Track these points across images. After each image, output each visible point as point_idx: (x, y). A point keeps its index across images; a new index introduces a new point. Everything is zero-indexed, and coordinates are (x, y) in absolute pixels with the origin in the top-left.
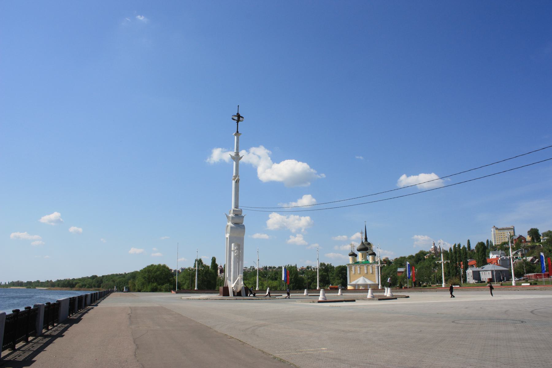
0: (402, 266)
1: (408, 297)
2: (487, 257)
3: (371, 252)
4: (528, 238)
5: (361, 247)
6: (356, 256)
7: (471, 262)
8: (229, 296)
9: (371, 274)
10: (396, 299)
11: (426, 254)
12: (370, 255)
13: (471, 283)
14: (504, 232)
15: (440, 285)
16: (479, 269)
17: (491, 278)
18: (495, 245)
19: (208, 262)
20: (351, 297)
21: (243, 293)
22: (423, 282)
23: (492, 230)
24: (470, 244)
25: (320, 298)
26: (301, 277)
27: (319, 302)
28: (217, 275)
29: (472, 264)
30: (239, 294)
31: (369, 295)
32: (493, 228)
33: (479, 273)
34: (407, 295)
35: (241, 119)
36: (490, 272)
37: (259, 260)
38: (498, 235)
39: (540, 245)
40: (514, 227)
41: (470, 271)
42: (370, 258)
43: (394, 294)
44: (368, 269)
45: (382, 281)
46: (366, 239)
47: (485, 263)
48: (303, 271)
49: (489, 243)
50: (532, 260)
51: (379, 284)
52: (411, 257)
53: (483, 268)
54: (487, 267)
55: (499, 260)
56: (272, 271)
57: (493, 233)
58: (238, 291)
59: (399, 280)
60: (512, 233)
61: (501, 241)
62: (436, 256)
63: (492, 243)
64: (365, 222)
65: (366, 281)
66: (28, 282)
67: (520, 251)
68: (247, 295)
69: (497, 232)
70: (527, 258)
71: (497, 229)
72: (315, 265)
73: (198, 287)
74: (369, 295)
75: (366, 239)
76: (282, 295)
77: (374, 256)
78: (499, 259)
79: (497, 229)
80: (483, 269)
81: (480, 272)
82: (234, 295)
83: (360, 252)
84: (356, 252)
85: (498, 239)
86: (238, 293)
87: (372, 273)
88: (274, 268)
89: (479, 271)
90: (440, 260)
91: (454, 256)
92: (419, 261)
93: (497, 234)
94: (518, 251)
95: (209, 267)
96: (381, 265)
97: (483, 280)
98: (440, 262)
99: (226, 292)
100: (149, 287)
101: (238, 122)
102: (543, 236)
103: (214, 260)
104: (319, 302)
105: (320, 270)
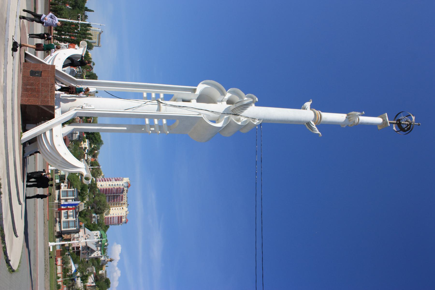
14: (97, 38)
23: (100, 30)
24: (90, 11)
32: (101, 31)
38: (95, 33)
40: (100, 47)
49: (89, 28)
55: (73, 69)
57: (97, 29)
60: (95, 45)
67: (80, 71)
69: (98, 33)
71: (100, 33)
79: (100, 33)
91: (80, 35)
93: (96, 38)
94: (80, 69)
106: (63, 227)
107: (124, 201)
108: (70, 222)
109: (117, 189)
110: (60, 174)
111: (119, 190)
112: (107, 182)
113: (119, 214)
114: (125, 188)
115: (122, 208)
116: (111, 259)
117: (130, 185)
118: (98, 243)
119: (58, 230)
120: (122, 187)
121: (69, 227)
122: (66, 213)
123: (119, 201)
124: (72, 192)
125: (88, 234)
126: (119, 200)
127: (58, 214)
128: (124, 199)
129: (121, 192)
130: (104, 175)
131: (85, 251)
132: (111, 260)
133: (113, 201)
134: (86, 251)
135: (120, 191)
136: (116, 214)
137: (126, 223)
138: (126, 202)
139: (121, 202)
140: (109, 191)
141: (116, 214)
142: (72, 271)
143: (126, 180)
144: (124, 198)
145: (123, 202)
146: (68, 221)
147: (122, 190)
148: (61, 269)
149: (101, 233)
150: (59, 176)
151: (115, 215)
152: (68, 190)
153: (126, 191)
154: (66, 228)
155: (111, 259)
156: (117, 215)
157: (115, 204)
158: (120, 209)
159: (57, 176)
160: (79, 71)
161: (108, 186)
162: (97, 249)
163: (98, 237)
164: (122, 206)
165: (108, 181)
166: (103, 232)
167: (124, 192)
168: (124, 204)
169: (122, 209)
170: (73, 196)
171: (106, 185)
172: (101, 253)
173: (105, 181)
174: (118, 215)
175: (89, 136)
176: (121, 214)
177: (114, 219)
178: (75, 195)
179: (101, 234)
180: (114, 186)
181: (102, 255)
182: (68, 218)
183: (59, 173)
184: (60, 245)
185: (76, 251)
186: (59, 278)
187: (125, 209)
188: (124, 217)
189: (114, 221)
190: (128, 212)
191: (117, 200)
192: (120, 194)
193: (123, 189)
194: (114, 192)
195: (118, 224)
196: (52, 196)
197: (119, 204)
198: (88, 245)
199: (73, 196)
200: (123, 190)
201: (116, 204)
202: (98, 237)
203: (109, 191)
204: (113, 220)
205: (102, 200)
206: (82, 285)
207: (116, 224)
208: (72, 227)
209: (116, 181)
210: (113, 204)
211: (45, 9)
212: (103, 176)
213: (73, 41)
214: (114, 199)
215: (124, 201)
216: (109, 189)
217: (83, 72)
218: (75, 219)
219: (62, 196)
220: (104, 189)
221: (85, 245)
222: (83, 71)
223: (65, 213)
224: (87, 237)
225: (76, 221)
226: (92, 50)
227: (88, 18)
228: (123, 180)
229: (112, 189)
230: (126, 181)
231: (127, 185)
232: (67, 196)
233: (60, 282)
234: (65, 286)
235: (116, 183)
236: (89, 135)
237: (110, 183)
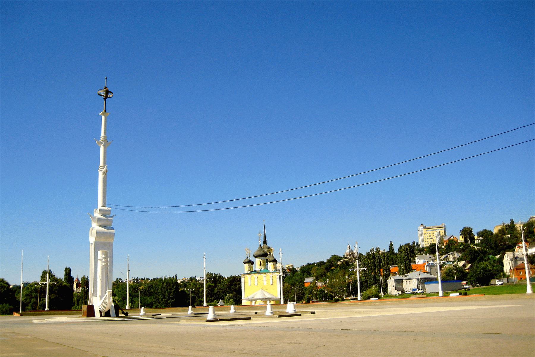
0: (309, 275)
1: (314, 313)
2: (412, 262)
3: (271, 259)
4: (461, 239)
5: (257, 253)
6: (252, 263)
7: (393, 268)
8: (95, 316)
9: (114, 229)
10: (300, 315)
11: (340, 260)
12: (270, 262)
14: (433, 231)
15: (356, 298)
16: (401, 277)
18: (422, 247)
19: (60, 275)
20: (415, 305)
21: (113, 312)
22: (336, 295)
25: (210, 316)
26: (183, 291)
27: (208, 321)
28: (73, 291)
29: (394, 271)
30: (107, 314)
31: (268, 311)
34: (313, 311)
35: (110, 95)
36: (416, 280)
37: (129, 270)
39: (474, 246)
41: (391, 281)
42: (271, 265)
43: (298, 310)
45: (284, 295)
46: (265, 242)
47: (409, 269)
48: (185, 284)
50: (464, 266)
51: (281, 298)
52: (321, 264)
54: (411, 275)
55: (426, 266)
56: (145, 283)
58: (106, 310)
59: (307, 293)
60: (443, 232)
61: (430, 243)
63: (419, 245)
65: (264, 295)
68: (117, 315)
70: (459, 263)
72: (201, 276)
73: (49, 307)
74: (268, 311)
75: (265, 242)
76: (160, 315)
77: (275, 263)
78: (427, 265)
80: (407, 278)
82: (101, 316)
84: (252, 259)
85: (427, 240)
86: (106, 313)
88: (148, 279)
90: (355, 267)
95: (61, 280)
96: (284, 275)
98: (355, 270)
99: (90, 312)
101: (105, 99)
102: (479, 236)
103: (68, 271)
104: (208, 321)
105: (207, 282)
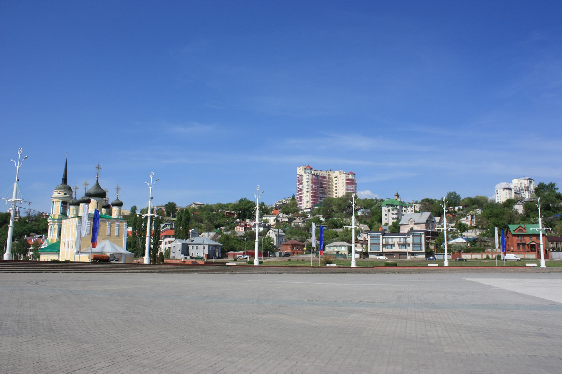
13: (178, 258)
17: (207, 254)
33: (356, 258)
44: (112, 227)
53: (192, 241)
62: (29, 220)
64: (67, 153)
65: (116, 249)
66: (70, 261)
67: (170, 224)
81: (189, 246)
83: (94, 199)
87: (118, 236)
89: (188, 244)
92: (4, 225)
97: (192, 255)
100: (251, 204)
106: (378, 250)
107: (326, 175)
108: (415, 242)
109: (313, 183)
110: (347, 253)
111: (315, 180)
112: (303, 195)
113: (343, 183)
114: (311, 173)
115: (335, 178)
116: (395, 196)
117: (308, 166)
118: (399, 209)
119: (423, 256)
120: (311, 177)
121: (421, 244)
122: (400, 246)
123: (326, 182)
124: (373, 238)
125: (409, 221)
126: (324, 181)
127: (402, 256)
128: (324, 174)
129: (316, 178)
130: (284, 199)
131: (430, 226)
132: (397, 196)
133: (326, 188)
134: (431, 224)
135: (315, 179)
136: (343, 186)
137: (354, 174)
138: (327, 172)
139: (327, 178)
140: (314, 193)
141: (343, 186)
142: (462, 242)
143: (300, 171)
144: (323, 175)
145: (327, 176)
146: (412, 244)
147: (314, 177)
148: (477, 254)
149: (385, 205)
150: (348, 253)
151: (344, 188)
152: (370, 244)
153: (316, 172)
154: (379, 247)
155: (395, 196)
156: (344, 184)
157: (329, 186)
158: (336, 180)
159: (349, 256)
160: (170, 225)
161: (308, 194)
162: (404, 211)
163: (392, 209)
164: (331, 178)
165: (301, 194)
166: (384, 203)
167: (317, 174)
168: (329, 175)
169: (336, 179)
170: (378, 237)
171: (307, 196)
172: (410, 207)
173: (301, 197)
174: (345, 183)
175: (247, 215)
176: (343, 179)
177: (349, 189)
178: (377, 235)
179: (387, 205)
180: (309, 187)
181: (413, 206)
182: (409, 244)
183: (344, 253)
184: (448, 255)
185: (432, 236)
186: (488, 257)
187: (337, 173)
188: (347, 177)
189: (352, 189)
190: (341, 170)
191: (325, 184)
192: (318, 180)
193: (313, 175)
194: (316, 187)
195: (354, 184)
196: (398, 262)
197: (329, 182)
198: (425, 222)
199: (378, 237)
200: (314, 175)
201: (329, 185)
202: (392, 209)
203: (314, 193)
204: (350, 191)
205: (338, 202)
206: (470, 231)
207: (355, 187)
208: (421, 240)
209: (302, 183)
210: (329, 189)
211: (294, 273)
212: (286, 200)
213: (157, 233)
214: (323, 187)
215: (326, 175)
216: (312, 193)
217: (169, 221)
218: (411, 236)
219: (422, 250)
220: (312, 200)
221: (424, 225)
222: (166, 220)
223: (400, 248)
224: (413, 223)
225: (413, 234)
226: (176, 204)
227: (137, 209)
228: (301, 175)
229: (312, 189)
230: (303, 171)
231: (309, 170)
232: (378, 244)
233: (492, 256)
234: (486, 250)
235: (305, 184)
236: (246, 215)
237: (304, 191)
